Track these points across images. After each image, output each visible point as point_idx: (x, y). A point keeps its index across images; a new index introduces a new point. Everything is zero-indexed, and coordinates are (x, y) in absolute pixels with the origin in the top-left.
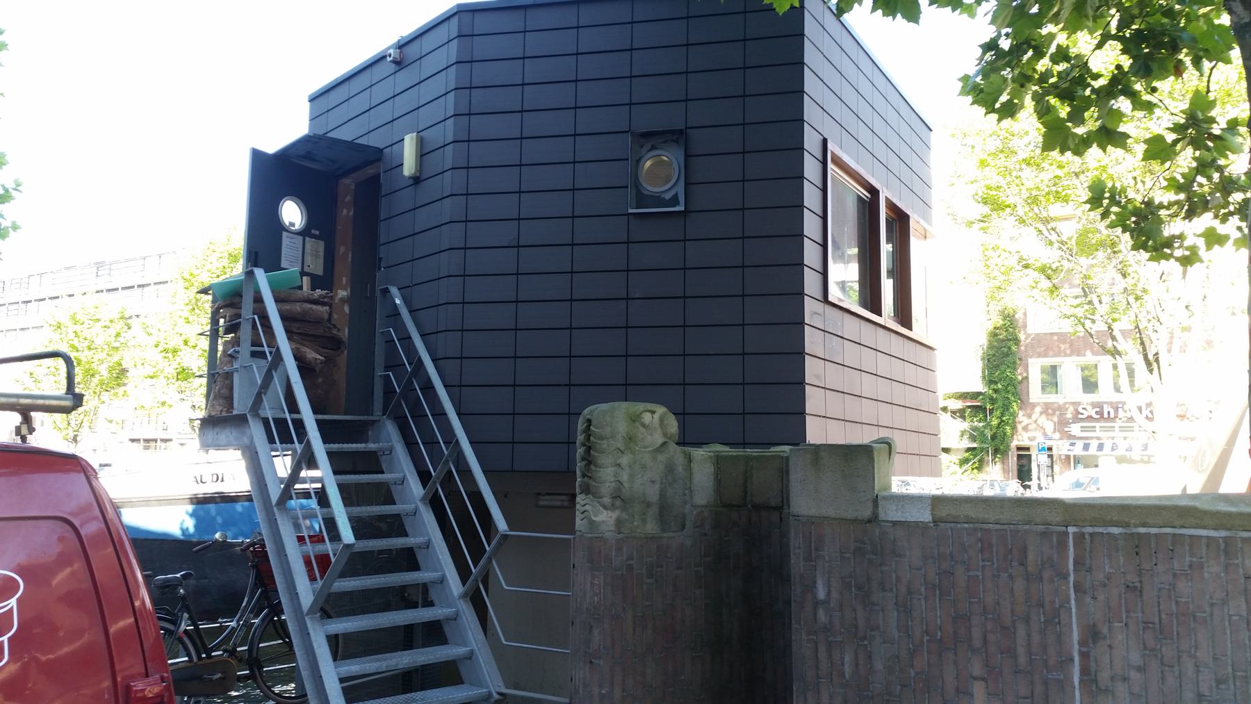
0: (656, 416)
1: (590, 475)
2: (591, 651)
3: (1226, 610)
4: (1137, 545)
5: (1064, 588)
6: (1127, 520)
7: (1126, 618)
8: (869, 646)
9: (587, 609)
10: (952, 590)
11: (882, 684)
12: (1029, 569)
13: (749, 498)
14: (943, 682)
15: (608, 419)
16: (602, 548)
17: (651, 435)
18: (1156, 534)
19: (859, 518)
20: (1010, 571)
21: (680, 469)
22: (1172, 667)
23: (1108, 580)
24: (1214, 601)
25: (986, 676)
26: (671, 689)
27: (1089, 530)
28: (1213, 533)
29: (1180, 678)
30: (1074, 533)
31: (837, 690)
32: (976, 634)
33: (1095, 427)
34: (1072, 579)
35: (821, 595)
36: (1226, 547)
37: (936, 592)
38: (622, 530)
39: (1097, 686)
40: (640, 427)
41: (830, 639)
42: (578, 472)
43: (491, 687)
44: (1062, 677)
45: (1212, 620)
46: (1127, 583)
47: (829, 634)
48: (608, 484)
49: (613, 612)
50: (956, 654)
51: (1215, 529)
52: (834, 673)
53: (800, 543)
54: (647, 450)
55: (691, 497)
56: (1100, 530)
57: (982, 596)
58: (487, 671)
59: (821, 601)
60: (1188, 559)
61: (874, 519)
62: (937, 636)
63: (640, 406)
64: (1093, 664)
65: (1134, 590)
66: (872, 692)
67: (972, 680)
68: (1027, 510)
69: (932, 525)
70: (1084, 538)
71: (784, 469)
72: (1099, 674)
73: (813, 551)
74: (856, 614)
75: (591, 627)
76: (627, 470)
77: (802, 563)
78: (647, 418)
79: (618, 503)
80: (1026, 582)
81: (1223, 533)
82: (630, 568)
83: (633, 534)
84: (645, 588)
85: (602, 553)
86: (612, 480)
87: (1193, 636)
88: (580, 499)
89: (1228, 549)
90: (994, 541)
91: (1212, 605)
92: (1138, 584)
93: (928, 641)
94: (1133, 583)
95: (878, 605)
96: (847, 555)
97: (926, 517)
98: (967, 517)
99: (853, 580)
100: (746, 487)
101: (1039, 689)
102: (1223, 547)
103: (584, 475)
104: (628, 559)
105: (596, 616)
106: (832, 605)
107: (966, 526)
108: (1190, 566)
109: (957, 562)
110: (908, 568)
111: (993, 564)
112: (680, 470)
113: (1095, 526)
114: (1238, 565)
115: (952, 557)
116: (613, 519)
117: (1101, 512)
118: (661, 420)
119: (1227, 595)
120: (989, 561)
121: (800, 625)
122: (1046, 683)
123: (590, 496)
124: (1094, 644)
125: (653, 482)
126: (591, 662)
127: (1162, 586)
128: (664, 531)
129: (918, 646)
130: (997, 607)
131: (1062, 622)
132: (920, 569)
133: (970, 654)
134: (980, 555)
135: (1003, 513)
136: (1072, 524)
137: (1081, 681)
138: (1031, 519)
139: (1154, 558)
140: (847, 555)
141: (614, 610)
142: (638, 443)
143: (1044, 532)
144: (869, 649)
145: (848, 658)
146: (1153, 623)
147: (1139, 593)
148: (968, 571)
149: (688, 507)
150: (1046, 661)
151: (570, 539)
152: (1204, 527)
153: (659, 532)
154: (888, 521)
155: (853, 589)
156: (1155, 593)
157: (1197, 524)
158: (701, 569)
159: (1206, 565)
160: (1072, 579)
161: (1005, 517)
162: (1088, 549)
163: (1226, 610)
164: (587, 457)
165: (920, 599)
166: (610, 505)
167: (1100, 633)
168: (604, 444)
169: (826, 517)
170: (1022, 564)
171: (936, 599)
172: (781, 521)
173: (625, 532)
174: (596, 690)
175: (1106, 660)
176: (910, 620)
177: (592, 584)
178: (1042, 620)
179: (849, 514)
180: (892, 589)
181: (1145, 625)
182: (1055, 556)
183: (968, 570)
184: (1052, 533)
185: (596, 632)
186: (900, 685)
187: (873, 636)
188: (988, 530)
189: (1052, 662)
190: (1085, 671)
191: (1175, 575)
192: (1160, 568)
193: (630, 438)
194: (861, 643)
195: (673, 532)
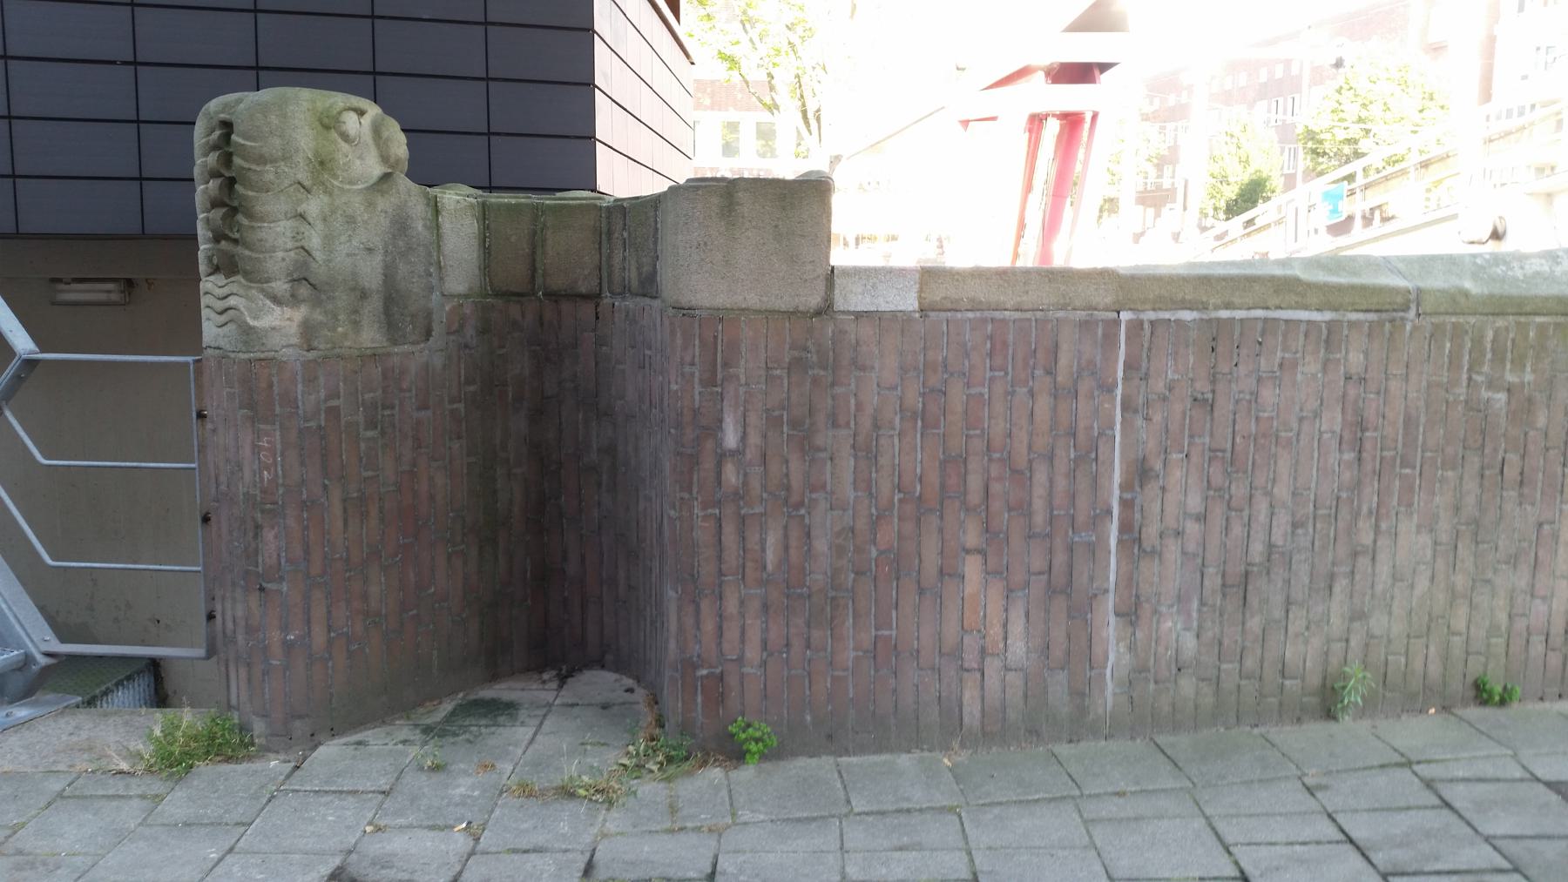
0: (367, 120)
1: (237, 236)
2: (260, 569)
3: (1317, 425)
4: (1216, 336)
5: (1106, 406)
6: (1204, 299)
7: (1188, 446)
8: (807, 516)
9: (246, 494)
10: (942, 418)
11: (826, 573)
12: (1059, 379)
13: (539, 280)
14: (920, 561)
15: (274, 120)
16: (275, 380)
17: (361, 158)
18: (1242, 320)
19: (801, 308)
20: (1031, 383)
21: (419, 226)
22: (1241, 511)
23: (1170, 391)
24: (1305, 414)
25: (984, 546)
26: (415, 612)
27: (1151, 315)
28: (1315, 316)
29: (1249, 525)
30: (1129, 322)
31: (752, 591)
32: (975, 482)
34: (1119, 391)
35: (731, 439)
36: (1328, 337)
37: (917, 423)
38: (315, 344)
39: (1140, 547)
40: (340, 140)
42: (202, 232)
43: (30, 645)
44: (1094, 538)
45: (1298, 441)
46: (1195, 394)
47: (742, 503)
48: (280, 254)
49: (305, 497)
50: (942, 518)
51: (1318, 310)
52: (749, 564)
53: (694, 357)
54: (355, 187)
55: (441, 279)
56: (1166, 315)
57: (986, 426)
58: (16, 617)
59: (730, 451)
60: (1279, 354)
61: (826, 309)
62: (915, 492)
63: (339, 100)
64: (1137, 516)
65: (1205, 404)
66: (809, 587)
67: (963, 554)
68: (1063, 288)
69: (917, 315)
70: (1142, 329)
71: (604, 230)
72: (1144, 530)
73: (719, 366)
74: (787, 468)
75: (258, 528)
76: (319, 225)
77: (698, 389)
78: (351, 120)
79: (304, 291)
80: (1052, 400)
81: (1328, 316)
82: (333, 412)
83: (337, 351)
84: (363, 446)
85: (276, 389)
86: (290, 245)
87: (1272, 466)
88: (211, 285)
89: (1331, 337)
90: (1011, 338)
91: (1301, 420)
92: (1210, 396)
93: (900, 501)
94: (1203, 394)
95: (826, 449)
96: (778, 372)
97: (910, 303)
98: (972, 300)
99: (785, 413)
100: (534, 260)
101: (1060, 559)
102: (1324, 337)
103: (218, 237)
104: (329, 398)
105: (268, 506)
106: (748, 456)
107: (970, 315)
108: (1281, 365)
109: (952, 374)
110: (875, 386)
111: (1007, 374)
112: (420, 228)
113: (1160, 309)
114: (1339, 360)
115: (946, 366)
116: (295, 325)
117: (1168, 288)
118: (377, 130)
119: (1321, 404)
120: (1001, 370)
122: (1070, 549)
123: (239, 278)
124: (1141, 487)
125: (370, 250)
126: (262, 589)
127: (1241, 396)
128: (394, 342)
129: (885, 511)
130: (1008, 440)
131: (1101, 457)
132: (894, 388)
133: (962, 515)
134: (988, 361)
135: (1027, 292)
136: (1127, 307)
137: (1120, 542)
138: (1068, 301)
139: (1235, 356)
140: (778, 372)
141: (305, 492)
142: (339, 172)
143: (1087, 322)
144: (807, 521)
145: (773, 539)
146: (1224, 451)
147: (1209, 408)
149: (436, 296)
150: (1073, 518)
151: (187, 364)
152: (1306, 308)
153: (385, 345)
154: (849, 313)
155: (785, 425)
156: (1231, 407)
157: (1297, 302)
158: (461, 406)
159: (1301, 362)
160: (1119, 391)
161: (1028, 300)
162: (1146, 345)
163: (1317, 425)
164: (227, 201)
165: (892, 436)
166: (288, 295)
167: (1152, 469)
168: (269, 173)
169: (743, 310)
170: (1049, 372)
171: (916, 436)
172: (597, 318)
173: (322, 347)
174: (275, 636)
175: (1157, 507)
176: (874, 470)
177: (256, 449)
178: (1072, 456)
179: (782, 304)
180: (848, 423)
181: (1212, 454)
182: (1098, 358)
183: (968, 385)
184: (1096, 322)
185: (269, 535)
186: (853, 571)
187: (814, 500)
188: (1003, 321)
189: (1081, 519)
190: (1125, 527)
191: (1259, 380)
192: (1242, 370)
193: (322, 163)
194: (794, 513)
195: (413, 343)
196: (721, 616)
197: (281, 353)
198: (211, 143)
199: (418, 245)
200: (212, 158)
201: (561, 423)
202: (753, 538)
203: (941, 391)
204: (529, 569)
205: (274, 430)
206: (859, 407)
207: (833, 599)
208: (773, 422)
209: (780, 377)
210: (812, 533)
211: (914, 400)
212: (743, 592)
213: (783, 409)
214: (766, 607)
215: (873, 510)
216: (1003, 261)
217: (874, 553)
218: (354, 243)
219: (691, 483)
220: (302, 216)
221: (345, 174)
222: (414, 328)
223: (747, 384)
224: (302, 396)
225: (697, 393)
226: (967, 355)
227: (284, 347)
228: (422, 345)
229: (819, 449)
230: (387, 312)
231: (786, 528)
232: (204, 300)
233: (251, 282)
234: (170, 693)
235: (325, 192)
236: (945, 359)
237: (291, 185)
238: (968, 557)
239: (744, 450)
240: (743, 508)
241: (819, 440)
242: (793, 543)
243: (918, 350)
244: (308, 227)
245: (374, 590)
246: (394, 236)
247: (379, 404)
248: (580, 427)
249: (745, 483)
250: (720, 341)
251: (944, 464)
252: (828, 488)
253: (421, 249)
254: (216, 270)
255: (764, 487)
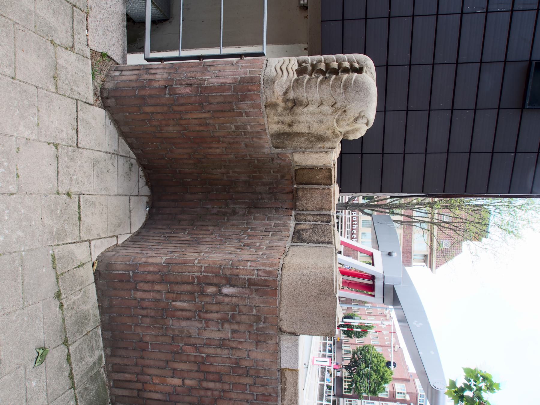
10: (237, 374)
14: (179, 362)
16: (252, 93)
32: (211, 385)
33: (349, 228)
35: (226, 290)
41: (196, 294)
48: (305, 95)
50: (196, 371)
52: (175, 295)
53: (261, 276)
76: (318, 110)
79: (290, 104)
84: (228, 125)
86: (309, 99)
93: (203, 357)
95: (222, 328)
98: (285, 389)
99: (237, 313)
103: (314, 66)
111: (255, 400)
116: (276, 101)
120: (256, 398)
121: (204, 272)
128: (272, 136)
130: (228, 399)
134: (260, 393)
144: (193, 319)
148: (249, 385)
153: (270, 133)
155: (232, 313)
158: (248, 158)
166: (288, 98)
180: (233, 338)
185: (188, 90)
188: (277, 401)
193: (345, 111)
195: (272, 142)
196: (154, 282)
197: (264, 95)
198: (354, 63)
199: (313, 145)
200: (347, 64)
201: (244, 193)
202: (185, 297)
203: (248, 374)
204: (187, 180)
205: (231, 92)
206: (241, 342)
207: (162, 328)
208: (235, 307)
209: (252, 311)
210: (188, 321)
211: (244, 363)
212: (163, 292)
213: (239, 312)
214: (157, 300)
215: (198, 345)
216: (313, 336)
217: (181, 345)
218: (312, 122)
219: (207, 273)
220: (321, 104)
221: (340, 119)
222: (278, 143)
223: (249, 298)
224: (246, 103)
225: (245, 277)
226: (262, 386)
227: (266, 96)
228: (272, 146)
229: (223, 326)
230: (284, 134)
231: (190, 310)
232: (287, 59)
233: (293, 83)
234: (157, 25)
235: (332, 112)
236: (261, 377)
237: (335, 100)
238: (181, 380)
239: (222, 295)
240: (198, 294)
241: (227, 326)
242: (184, 313)
243: (264, 367)
244: (317, 106)
245: (171, 128)
246: (316, 136)
247: (245, 130)
248: (243, 201)
249: (207, 295)
250: (268, 288)
251: (218, 373)
252: (207, 328)
253: (311, 146)
254: (300, 64)
255: (207, 303)
